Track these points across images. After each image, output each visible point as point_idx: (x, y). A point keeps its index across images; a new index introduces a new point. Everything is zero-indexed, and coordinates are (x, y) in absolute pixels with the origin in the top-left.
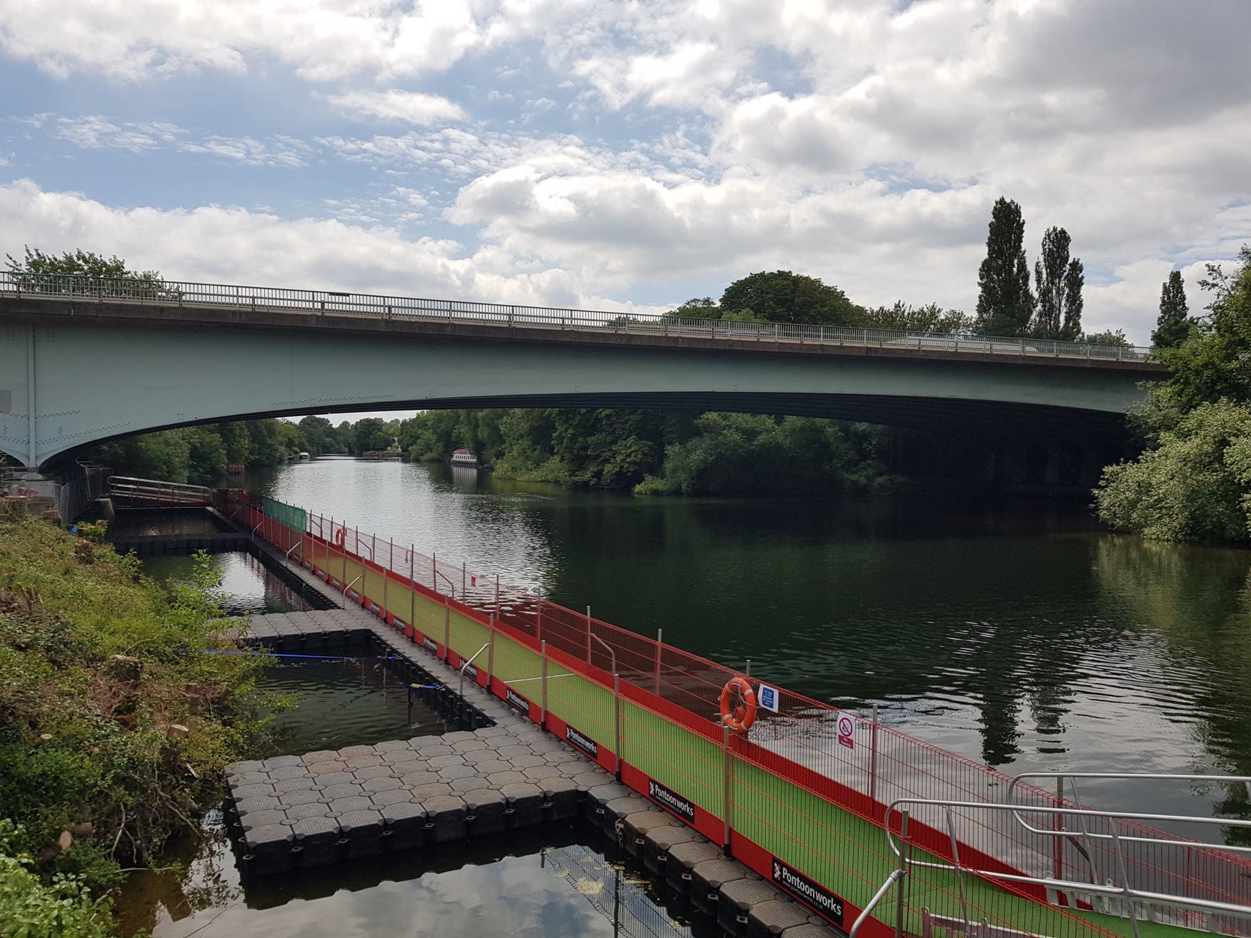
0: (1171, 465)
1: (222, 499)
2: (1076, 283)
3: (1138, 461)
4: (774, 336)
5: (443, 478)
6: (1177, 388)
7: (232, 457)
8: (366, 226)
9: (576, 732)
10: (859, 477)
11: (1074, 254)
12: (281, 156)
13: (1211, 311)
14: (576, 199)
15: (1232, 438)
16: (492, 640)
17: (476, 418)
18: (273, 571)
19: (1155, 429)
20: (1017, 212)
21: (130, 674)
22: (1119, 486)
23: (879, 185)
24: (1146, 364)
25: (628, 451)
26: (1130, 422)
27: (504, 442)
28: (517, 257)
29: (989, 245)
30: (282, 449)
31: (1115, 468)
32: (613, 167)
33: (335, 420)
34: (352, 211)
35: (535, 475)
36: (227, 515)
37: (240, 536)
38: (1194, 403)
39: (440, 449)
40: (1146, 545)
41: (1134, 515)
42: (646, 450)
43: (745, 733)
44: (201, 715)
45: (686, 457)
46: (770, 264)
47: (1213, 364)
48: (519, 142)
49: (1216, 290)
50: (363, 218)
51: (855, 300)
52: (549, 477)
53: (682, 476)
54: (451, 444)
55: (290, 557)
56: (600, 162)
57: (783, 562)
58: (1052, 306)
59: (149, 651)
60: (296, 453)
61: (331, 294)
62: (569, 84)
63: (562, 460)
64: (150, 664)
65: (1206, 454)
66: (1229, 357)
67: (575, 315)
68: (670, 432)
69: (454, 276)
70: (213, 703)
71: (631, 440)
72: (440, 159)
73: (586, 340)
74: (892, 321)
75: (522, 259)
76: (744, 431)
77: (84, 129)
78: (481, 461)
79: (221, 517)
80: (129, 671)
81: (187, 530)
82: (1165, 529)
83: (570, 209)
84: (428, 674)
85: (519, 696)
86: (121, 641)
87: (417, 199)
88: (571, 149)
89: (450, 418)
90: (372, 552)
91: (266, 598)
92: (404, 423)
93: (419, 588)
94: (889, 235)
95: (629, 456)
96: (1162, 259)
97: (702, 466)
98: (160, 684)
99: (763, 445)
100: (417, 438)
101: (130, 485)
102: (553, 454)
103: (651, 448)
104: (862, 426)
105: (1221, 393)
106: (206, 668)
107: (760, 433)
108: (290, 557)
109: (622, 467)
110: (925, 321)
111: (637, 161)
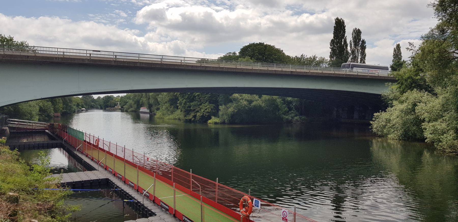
0: (397, 113)
1: (51, 127)
2: (363, 48)
3: (386, 111)
4: (258, 67)
5: (137, 118)
6: (398, 86)
7: (56, 111)
8: (105, 24)
9: (186, 217)
10: (289, 117)
11: (363, 37)
13: (410, 59)
14: (183, 15)
15: (418, 104)
16: (155, 183)
17: (149, 95)
18: (71, 155)
19: (391, 100)
20: (343, 22)
21: (15, 200)
22: (380, 120)
23: (291, 12)
24: (388, 77)
25: (206, 107)
26: (383, 97)
27: (159, 104)
28: (162, 36)
29: (334, 34)
30: (75, 107)
31: (378, 114)
33: (95, 97)
34: (99, 18)
35: (171, 117)
36: (53, 133)
37: (59, 142)
38: (405, 91)
39: (135, 107)
40: (389, 141)
41: (385, 131)
42: (212, 107)
43: (249, 217)
44: (43, 214)
45: (227, 110)
46: (256, 40)
47: (411, 77)
49: (412, 51)
50: (103, 21)
51: (287, 53)
52: (177, 117)
53: (225, 117)
54: (139, 105)
55: (78, 150)
57: (262, 149)
58: (355, 57)
59: (22, 190)
60: (80, 108)
61: (94, 51)
63: (181, 111)
64: (23, 195)
65: (409, 109)
66: (416, 75)
67: (186, 59)
68: (221, 101)
69: (139, 43)
70: (48, 209)
71: (207, 104)
73: (190, 68)
74: (300, 61)
75: (163, 37)
76: (248, 101)
78: (151, 111)
79: (51, 134)
80: (14, 199)
81: (38, 139)
82: (395, 135)
83: (179, 19)
84: (130, 196)
85: (165, 204)
86: (12, 186)
87: (124, 14)
89: (139, 95)
90: (109, 148)
91: (68, 166)
92: (122, 97)
93: (127, 162)
94: (296, 29)
96: (390, 39)
97: (233, 113)
98: (27, 203)
99: (255, 106)
100: (127, 103)
101: (16, 122)
102: (178, 109)
103: (214, 107)
104: (289, 99)
105: (414, 87)
106: (45, 196)
107: (253, 101)
108: (78, 150)
109: (203, 114)
110: (311, 62)
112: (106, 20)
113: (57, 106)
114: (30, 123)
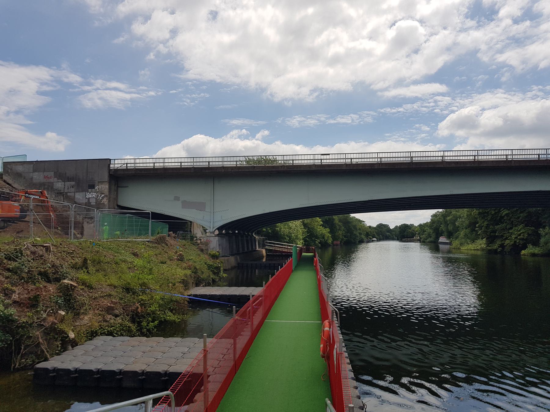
8: (404, 142)
12: (366, 119)
25: (519, 232)
32: (523, 100)
42: (530, 232)
48: (472, 97)
50: (402, 139)
56: (515, 98)
60: (371, 238)
61: (322, 155)
62: (494, 67)
72: (434, 109)
73: (453, 165)
77: (295, 121)
83: (499, 122)
88: (499, 95)
95: (520, 235)
109: (515, 242)
111: (536, 95)
112: (405, 138)
113: (337, 234)
114: (289, 246)
